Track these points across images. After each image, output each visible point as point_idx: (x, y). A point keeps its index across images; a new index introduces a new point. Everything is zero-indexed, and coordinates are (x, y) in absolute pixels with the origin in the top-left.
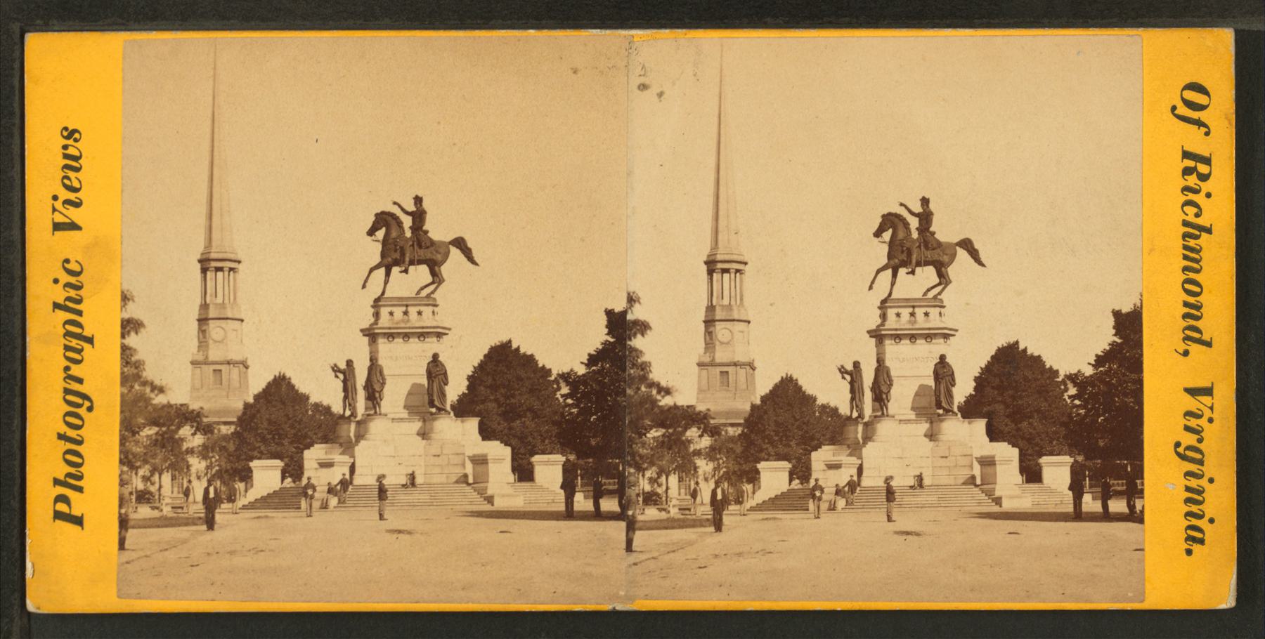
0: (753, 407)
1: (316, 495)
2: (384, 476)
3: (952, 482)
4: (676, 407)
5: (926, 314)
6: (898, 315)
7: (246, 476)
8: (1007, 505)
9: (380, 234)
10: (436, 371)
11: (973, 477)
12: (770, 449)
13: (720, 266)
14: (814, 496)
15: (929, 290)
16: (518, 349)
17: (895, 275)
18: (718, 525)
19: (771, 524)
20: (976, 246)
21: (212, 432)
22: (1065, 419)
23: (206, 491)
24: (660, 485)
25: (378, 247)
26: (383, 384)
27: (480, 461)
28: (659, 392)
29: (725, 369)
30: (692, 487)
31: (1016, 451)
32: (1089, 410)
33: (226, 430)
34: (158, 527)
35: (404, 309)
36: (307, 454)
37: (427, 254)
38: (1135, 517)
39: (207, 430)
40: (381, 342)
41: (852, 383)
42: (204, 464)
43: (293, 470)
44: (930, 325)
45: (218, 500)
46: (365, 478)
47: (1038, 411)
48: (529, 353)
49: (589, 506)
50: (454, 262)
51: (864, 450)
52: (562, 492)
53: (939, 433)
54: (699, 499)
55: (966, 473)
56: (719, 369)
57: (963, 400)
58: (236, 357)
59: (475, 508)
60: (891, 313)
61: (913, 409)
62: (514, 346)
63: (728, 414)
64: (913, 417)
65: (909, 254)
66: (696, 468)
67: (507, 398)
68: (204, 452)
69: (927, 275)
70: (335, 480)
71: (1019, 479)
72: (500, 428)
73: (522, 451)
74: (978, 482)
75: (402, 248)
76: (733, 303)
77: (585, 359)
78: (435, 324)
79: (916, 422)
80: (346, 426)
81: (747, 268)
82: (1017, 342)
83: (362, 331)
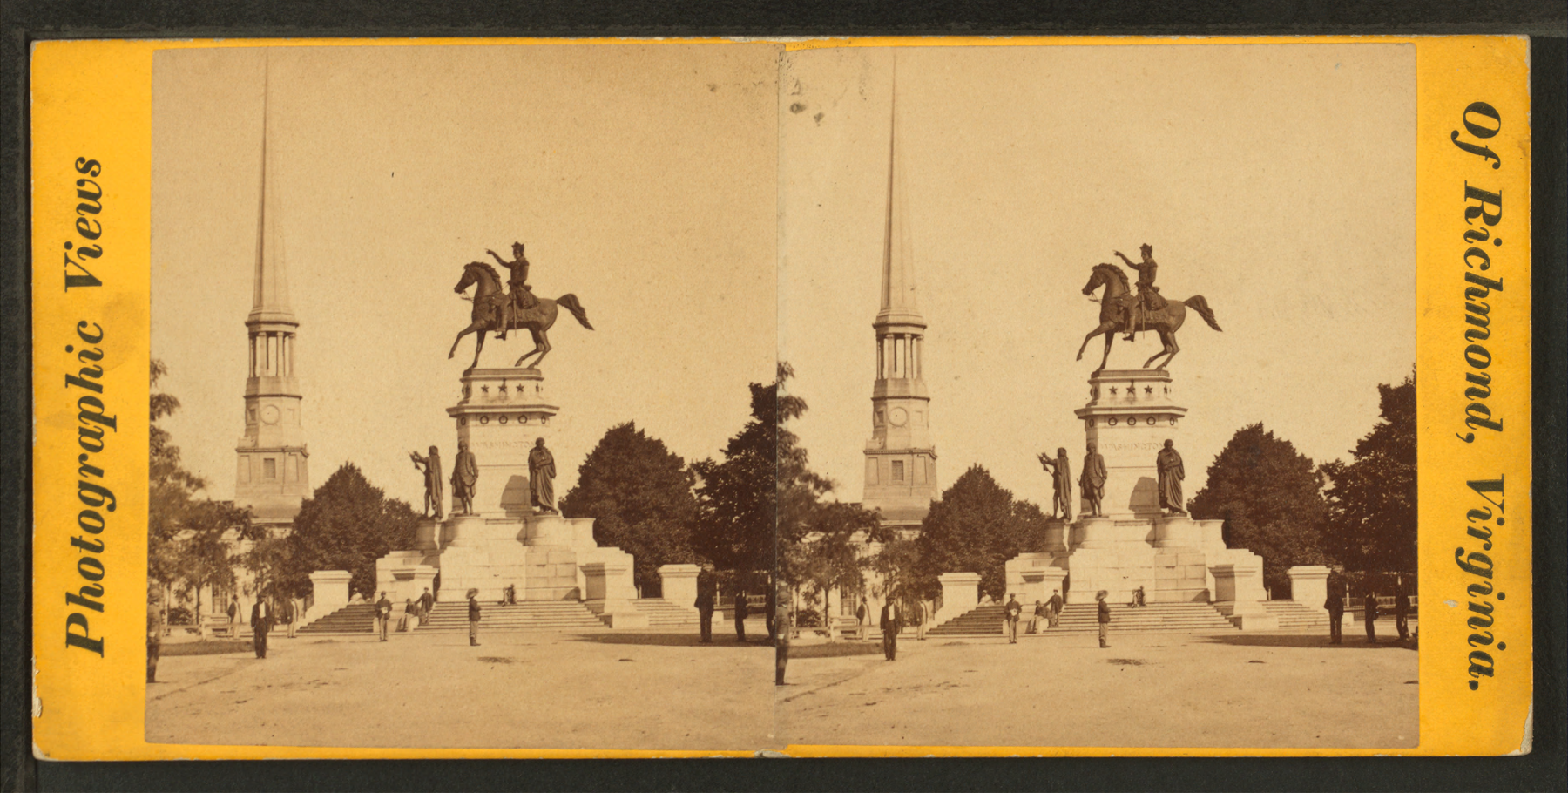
1: (392, 614)
4: (837, 505)
5: (1148, 390)
6: (1113, 391)
7: (305, 590)
8: (1249, 627)
9: (472, 290)
10: (540, 460)
11: (1207, 592)
12: (955, 557)
13: (892, 330)
14: (379, 614)
15: (1151, 360)
16: (642, 433)
18: (260, 649)
19: (955, 650)
21: (262, 536)
22: (1320, 520)
23: (256, 610)
25: (469, 307)
26: (475, 476)
27: (595, 572)
29: (899, 458)
32: (1349, 510)
33: (280, 534)
34: (196, 654)
35: (500, 383)
37: (529, 315)
38: (1407, 641)
39: (256, 533)
40: (473, 424)
41: (1056, 475)
42: (252, 576)
43: (364, 583)
45: (270, 621)
46: (452, 593)
49: (730, 627)
50: (563, 326)
51: (1071, 558)
53: (1164, 537)
54: (866, 619)
55: (1198, 587)
56: (891, 458)
57: (1193, 496)
58: (293, 443)
60: (1104, 388)
62: (1266, 431)
63: (902, 514)
64: (1132, 517)
65: (1127, 315)
66: (862, 581)
67: (629, 493)
68: (253, 561)
72: (620, 531)
74: (1213, 598)
75: (498, 308)
76: (281, 374)
77: (725, 445)
78: (539, 402)
79: (1135, 523)
80: (1056, 531)
81: (926, 333)
82: (1261, 425)
83: (448, 410)
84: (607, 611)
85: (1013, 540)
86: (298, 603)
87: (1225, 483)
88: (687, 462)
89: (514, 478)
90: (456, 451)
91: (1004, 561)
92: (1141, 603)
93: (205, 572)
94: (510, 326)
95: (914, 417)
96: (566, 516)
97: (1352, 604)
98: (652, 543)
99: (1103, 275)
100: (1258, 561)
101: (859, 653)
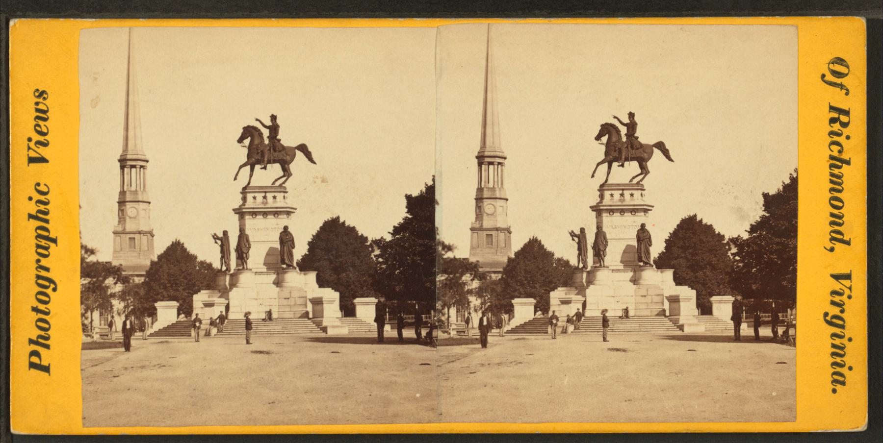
1: (202, 326)
3: (649, 314)
5: (274, 197)
6: (254, 198)
7: (153, 313)
8: (688, 330)
10: (286, 239)
11: (664, 311)
12: (165, 293)
13: (129, 163)
14: (195, 326)
16: (701, 221)
17: (252, 170)
18: (127, 346)
19: (164, 346)
20: (667, 147)
21: (485, 279)
23: (125, 323)
24: (87, 318)
25: (245, 151)
26: (606, 245)
27: (674, 300)
28: (443, 249)
30: (110, 319)
31: (694, 292)
33: (138, 280)
34: (91, 349)
36: (196, 297)
37: (280, 156)
38: (787, 340)
40: (247, 217)
41: (579, 243)
42: (122, 304)
43: (186, 308)
44: (636, 203)
45: (132, 330)
46: (236, 314)
47: (710, 263)
48: (709, 224)
49: (394, 334)
50: (657, 159)
51: (230, 293)
52: (732, 322)
53: (283, 280)
54: (114, 328)
55: (302, 310)
56: (485, 233)
57: (300, 258)
58: (145, 229)
59: (670, 333)
60: (607, 194)
62: (341, 220)
63: (134, 268)
64: (265, 270)
68: (123, 296)
69: (633, 167)
71: (696, 312)
72: (688, 277)
73: (704, 293)
74: (668, 314)
77: (391, 230)
78: (285, 205)
80: (222, 278)
81: (148, 165)
82: (695, 215)
83: (234, 210)
86: (505, 317)
87: (675, 248)
88: (727, 238)
89: (271, 248)
91: (192, 295)
92: (627, 316)
93: (95, 302)
95: (500, 210)
96: (658, 268)
97: (390, 319)
98: (349, 286)
100: (337, 295)
101: (110, 347)
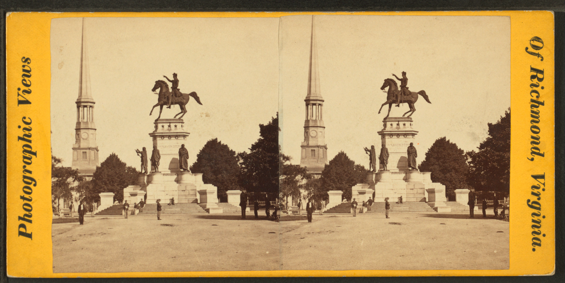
0: (98, 168)
1: (358, 207)
2: (388, 198)
4: (63, 168)
5: (176, 126)
6: (163, 126)
7: (98, 200)
8: (212, 212)
9: (387, 89)
11: (425, 198)
12: (105, 187)
13: (83, 104)
14: (124, 208)
15: (177, 115)
16: (449, 141)
18: (81, 221)
19: (105, 221)
20: (427, 94)
21: (311, 178)
22: (466, 172)
23: (80, 207)
24: (55, 203)
25: (157, 97)
26: (388, 157)
27: (431, 192)
29: (84, 151)
30: (70, 204)
31: (444, 186)
32: (248, 170)
33: (89, 179)
34: (58, 223)
35: (168, 124)
36: (125, 190)
38: (504, 217)
39: (80, 179)
40: (158, 139)
41: (370, 155)
42: (78, 194)
43: (119, 197)
45: (85, 211)
46: (151, 201)
47: (454, 168)
49: (252, 213)
50: (420, 102)
51: (147, 187)
52: (468, 206)
53: (181, 179)
54: (73, 209)
55: (193, 198)
58: (93, 146)
60: (388, 124)
61: (169, 169)
62: (218, 141)
64: (170, 173)
65: (168, 99)
66: (71, 196)
67: (443, 163)
68: (78, 189)
69: (405, 107)
70: (366, 200)
72: (440, 177)
74: (427, 200)
75: (168, 97)
76: (317, 119)
77: (250, 147)
78: (411, 130)
79: (399, 173)
80: (142, 177)
81: (95, 105)
82: (445, 138)
84: (436, 206)
85: (355, 179)
88: (465, 152)
89: (173, 159)
90: (152, 149)
92: (401, 202)
94: (172, 103)
95: (320, 134)
96: (421, 171)
99: (388, 83)
100: (215, 189)
